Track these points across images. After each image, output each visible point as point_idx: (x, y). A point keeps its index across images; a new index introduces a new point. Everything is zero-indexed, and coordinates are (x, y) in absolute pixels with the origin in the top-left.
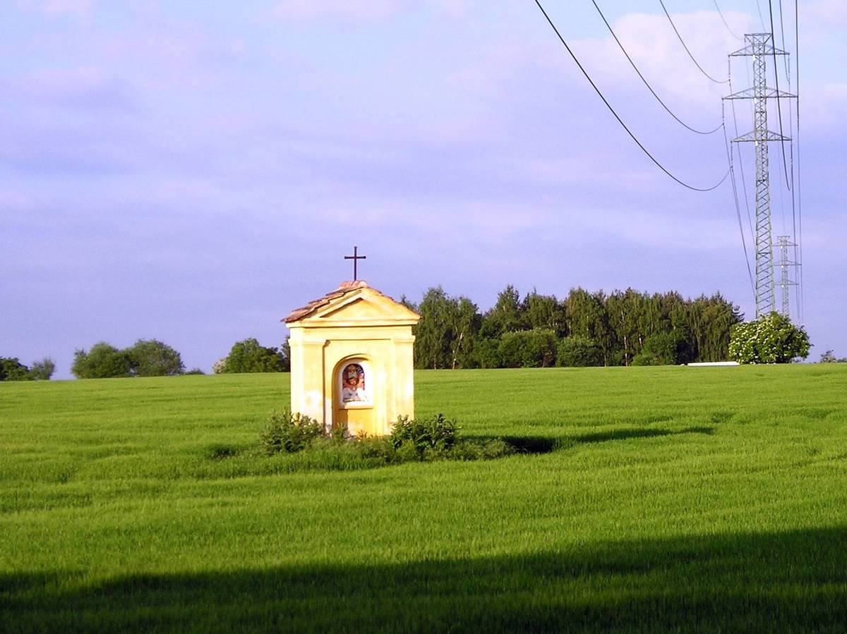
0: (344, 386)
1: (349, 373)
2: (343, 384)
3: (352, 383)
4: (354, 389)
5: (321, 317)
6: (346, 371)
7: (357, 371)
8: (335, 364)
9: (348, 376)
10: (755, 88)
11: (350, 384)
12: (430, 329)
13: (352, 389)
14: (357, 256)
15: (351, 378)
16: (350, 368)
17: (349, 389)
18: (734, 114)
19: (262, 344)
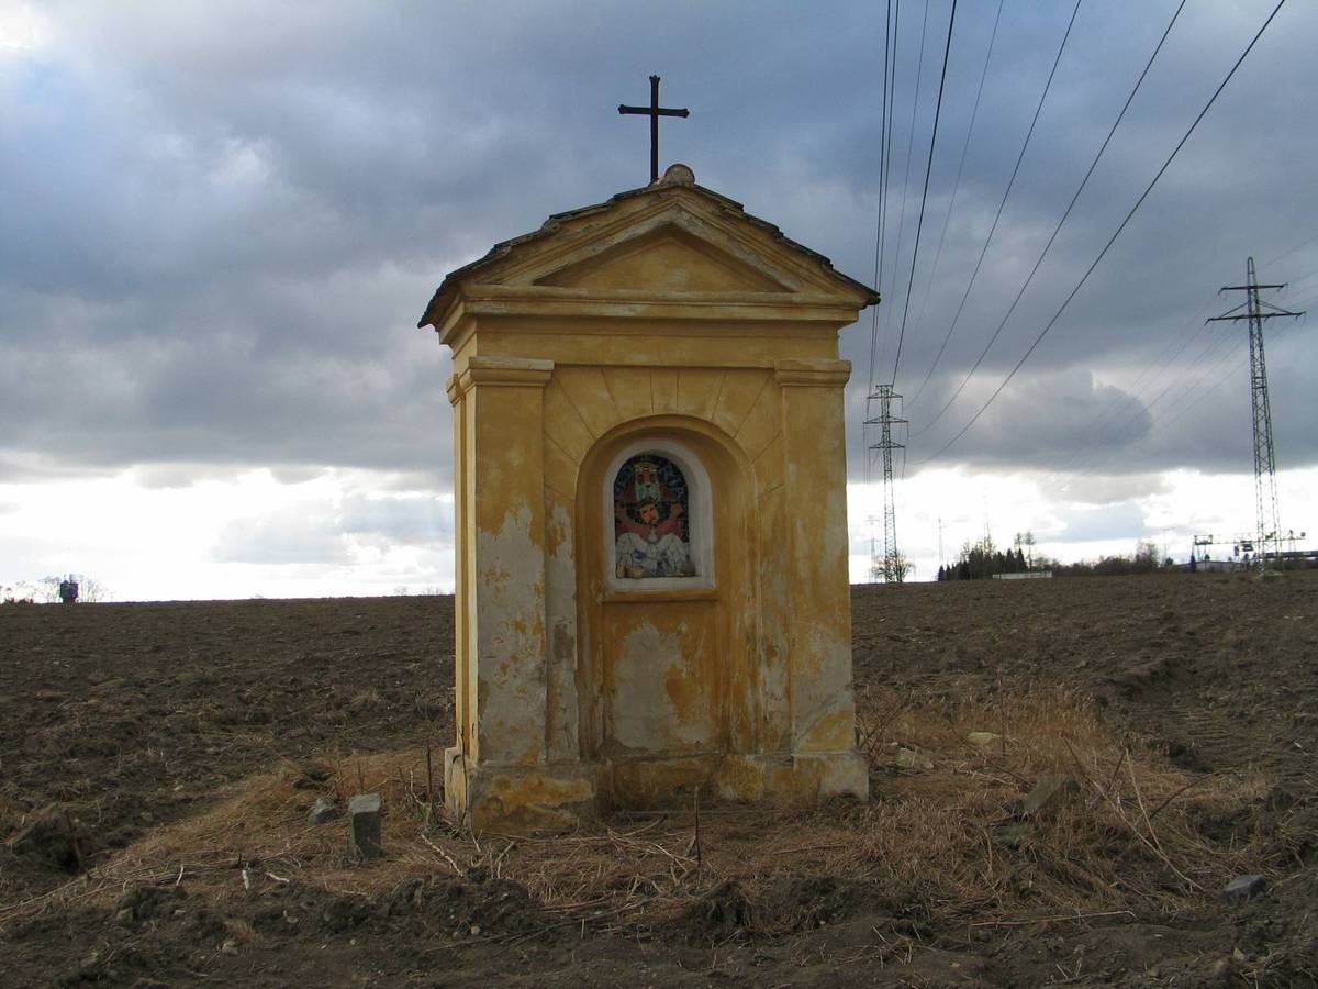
0: (620, 528)
1: (638, 486)
2: (617, 521)
3: (646, 518)
4: (653, 538)
5: (537, 282)
6: (625, 480)
7: (661, 477)
8: (350, 595)
9: (632, 494)
10: (882, 417)
11: (639, 520)
12: (524, 632)
13: (644, 537)
14: (661, 118)
15: (644, 503)
16: (639, 468)
17: (635, 537)
18: (1052, 322)
19: (746, 210)
